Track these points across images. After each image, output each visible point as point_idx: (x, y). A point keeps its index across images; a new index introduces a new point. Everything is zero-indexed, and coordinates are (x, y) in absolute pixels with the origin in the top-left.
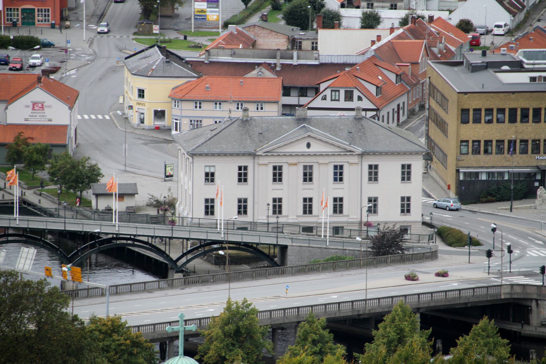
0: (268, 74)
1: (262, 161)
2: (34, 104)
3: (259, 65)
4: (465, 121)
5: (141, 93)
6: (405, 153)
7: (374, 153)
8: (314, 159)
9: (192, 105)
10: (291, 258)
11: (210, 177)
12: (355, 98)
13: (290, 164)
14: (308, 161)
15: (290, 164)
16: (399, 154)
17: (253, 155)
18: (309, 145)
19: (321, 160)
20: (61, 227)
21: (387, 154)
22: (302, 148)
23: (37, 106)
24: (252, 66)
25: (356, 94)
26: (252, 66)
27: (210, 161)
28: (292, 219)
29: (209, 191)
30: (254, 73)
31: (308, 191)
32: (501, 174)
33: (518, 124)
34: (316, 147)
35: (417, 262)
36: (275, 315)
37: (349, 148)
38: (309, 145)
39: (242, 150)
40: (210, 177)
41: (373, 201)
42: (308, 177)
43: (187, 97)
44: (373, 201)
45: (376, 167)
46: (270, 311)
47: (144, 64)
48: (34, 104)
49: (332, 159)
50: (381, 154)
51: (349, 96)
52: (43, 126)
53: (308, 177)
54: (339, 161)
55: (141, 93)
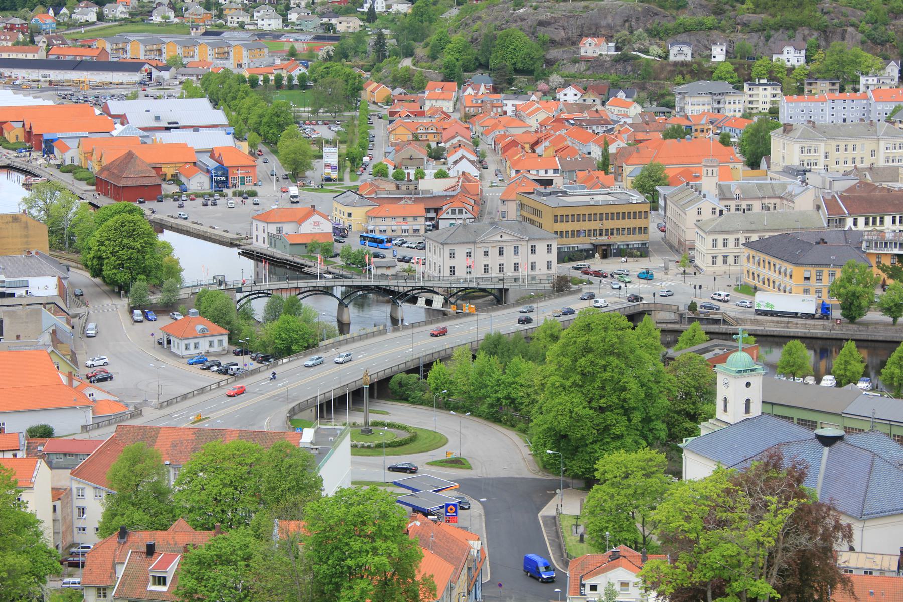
0: (410, 202)
1: (478, 246)
2: (314, 222)
3: (405, 198)
4: (556, 221)
5: (350, 215)
6: (549, 239)
7: (534, 239)
8: (504, 244)
9: (381, 219)
10: (511, 297)
11: (452, 255)
12: (464, 212)
13: (492, 247)
14: (501, 245)
15: (492, 247)
16: (546, 239)
17: (474, 243)
18: (501, 237)
19: (507, 244)
20: (351, 284)
21: (540, 239)
22: (498, 238)
23: (316, 223)
24: (401, 199)
25: (464, 210)
26: (401, 199)
27: (452, 247)
28: (509, 274)
29: (452, 263)
30: (403, 202)
31: (501, 260)
32: (574, 248)
33: (593, 222)
34: (505, 238)
35: (285, 360)
36: (408, 364)
37: (522, 237)
38: (501, 237)
39: (468, 241)
40: (452, 255)
41: (501, 265)
42: (501, 253)
43: (378, 215)
44: (501, 265)
45: (535, 246)
46: (446, 350)
47: (349, 200)
48: (314, 222)
49: (513, 243)
50: (537, 239)
51: (460, 212)
52: (319, 234)
53: (501, 253)
54: (516, 244)
55: (350, 215)
